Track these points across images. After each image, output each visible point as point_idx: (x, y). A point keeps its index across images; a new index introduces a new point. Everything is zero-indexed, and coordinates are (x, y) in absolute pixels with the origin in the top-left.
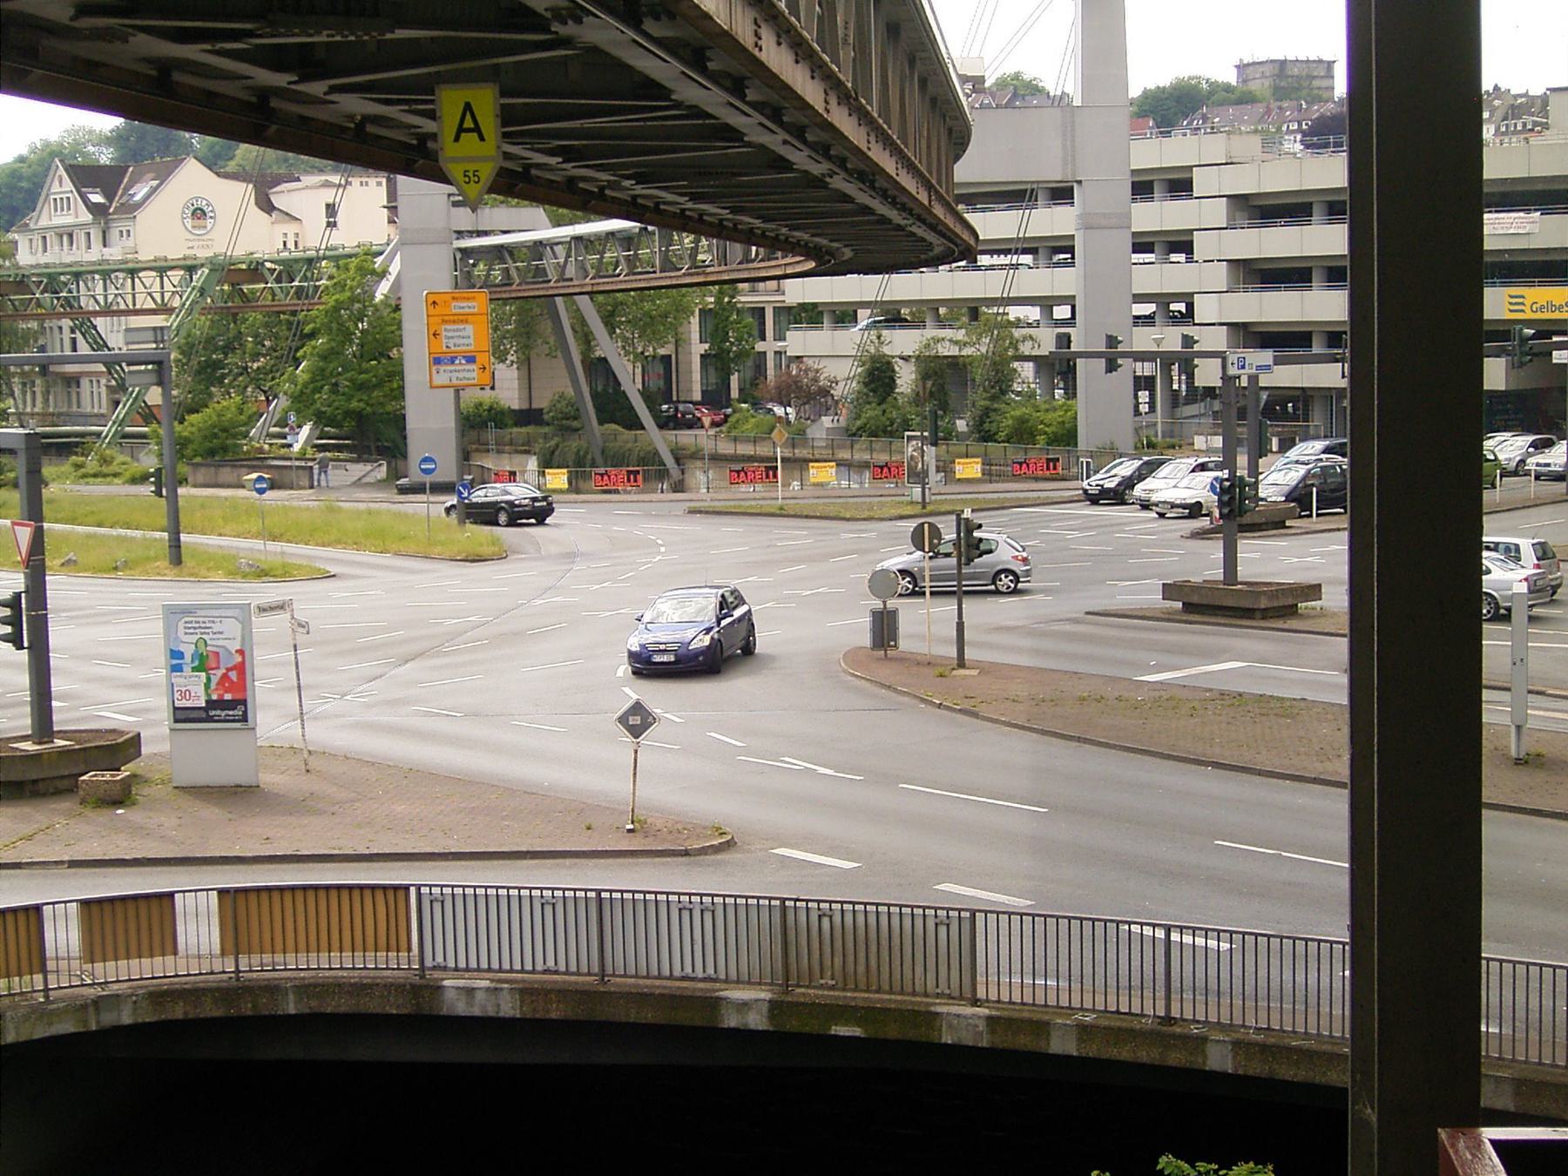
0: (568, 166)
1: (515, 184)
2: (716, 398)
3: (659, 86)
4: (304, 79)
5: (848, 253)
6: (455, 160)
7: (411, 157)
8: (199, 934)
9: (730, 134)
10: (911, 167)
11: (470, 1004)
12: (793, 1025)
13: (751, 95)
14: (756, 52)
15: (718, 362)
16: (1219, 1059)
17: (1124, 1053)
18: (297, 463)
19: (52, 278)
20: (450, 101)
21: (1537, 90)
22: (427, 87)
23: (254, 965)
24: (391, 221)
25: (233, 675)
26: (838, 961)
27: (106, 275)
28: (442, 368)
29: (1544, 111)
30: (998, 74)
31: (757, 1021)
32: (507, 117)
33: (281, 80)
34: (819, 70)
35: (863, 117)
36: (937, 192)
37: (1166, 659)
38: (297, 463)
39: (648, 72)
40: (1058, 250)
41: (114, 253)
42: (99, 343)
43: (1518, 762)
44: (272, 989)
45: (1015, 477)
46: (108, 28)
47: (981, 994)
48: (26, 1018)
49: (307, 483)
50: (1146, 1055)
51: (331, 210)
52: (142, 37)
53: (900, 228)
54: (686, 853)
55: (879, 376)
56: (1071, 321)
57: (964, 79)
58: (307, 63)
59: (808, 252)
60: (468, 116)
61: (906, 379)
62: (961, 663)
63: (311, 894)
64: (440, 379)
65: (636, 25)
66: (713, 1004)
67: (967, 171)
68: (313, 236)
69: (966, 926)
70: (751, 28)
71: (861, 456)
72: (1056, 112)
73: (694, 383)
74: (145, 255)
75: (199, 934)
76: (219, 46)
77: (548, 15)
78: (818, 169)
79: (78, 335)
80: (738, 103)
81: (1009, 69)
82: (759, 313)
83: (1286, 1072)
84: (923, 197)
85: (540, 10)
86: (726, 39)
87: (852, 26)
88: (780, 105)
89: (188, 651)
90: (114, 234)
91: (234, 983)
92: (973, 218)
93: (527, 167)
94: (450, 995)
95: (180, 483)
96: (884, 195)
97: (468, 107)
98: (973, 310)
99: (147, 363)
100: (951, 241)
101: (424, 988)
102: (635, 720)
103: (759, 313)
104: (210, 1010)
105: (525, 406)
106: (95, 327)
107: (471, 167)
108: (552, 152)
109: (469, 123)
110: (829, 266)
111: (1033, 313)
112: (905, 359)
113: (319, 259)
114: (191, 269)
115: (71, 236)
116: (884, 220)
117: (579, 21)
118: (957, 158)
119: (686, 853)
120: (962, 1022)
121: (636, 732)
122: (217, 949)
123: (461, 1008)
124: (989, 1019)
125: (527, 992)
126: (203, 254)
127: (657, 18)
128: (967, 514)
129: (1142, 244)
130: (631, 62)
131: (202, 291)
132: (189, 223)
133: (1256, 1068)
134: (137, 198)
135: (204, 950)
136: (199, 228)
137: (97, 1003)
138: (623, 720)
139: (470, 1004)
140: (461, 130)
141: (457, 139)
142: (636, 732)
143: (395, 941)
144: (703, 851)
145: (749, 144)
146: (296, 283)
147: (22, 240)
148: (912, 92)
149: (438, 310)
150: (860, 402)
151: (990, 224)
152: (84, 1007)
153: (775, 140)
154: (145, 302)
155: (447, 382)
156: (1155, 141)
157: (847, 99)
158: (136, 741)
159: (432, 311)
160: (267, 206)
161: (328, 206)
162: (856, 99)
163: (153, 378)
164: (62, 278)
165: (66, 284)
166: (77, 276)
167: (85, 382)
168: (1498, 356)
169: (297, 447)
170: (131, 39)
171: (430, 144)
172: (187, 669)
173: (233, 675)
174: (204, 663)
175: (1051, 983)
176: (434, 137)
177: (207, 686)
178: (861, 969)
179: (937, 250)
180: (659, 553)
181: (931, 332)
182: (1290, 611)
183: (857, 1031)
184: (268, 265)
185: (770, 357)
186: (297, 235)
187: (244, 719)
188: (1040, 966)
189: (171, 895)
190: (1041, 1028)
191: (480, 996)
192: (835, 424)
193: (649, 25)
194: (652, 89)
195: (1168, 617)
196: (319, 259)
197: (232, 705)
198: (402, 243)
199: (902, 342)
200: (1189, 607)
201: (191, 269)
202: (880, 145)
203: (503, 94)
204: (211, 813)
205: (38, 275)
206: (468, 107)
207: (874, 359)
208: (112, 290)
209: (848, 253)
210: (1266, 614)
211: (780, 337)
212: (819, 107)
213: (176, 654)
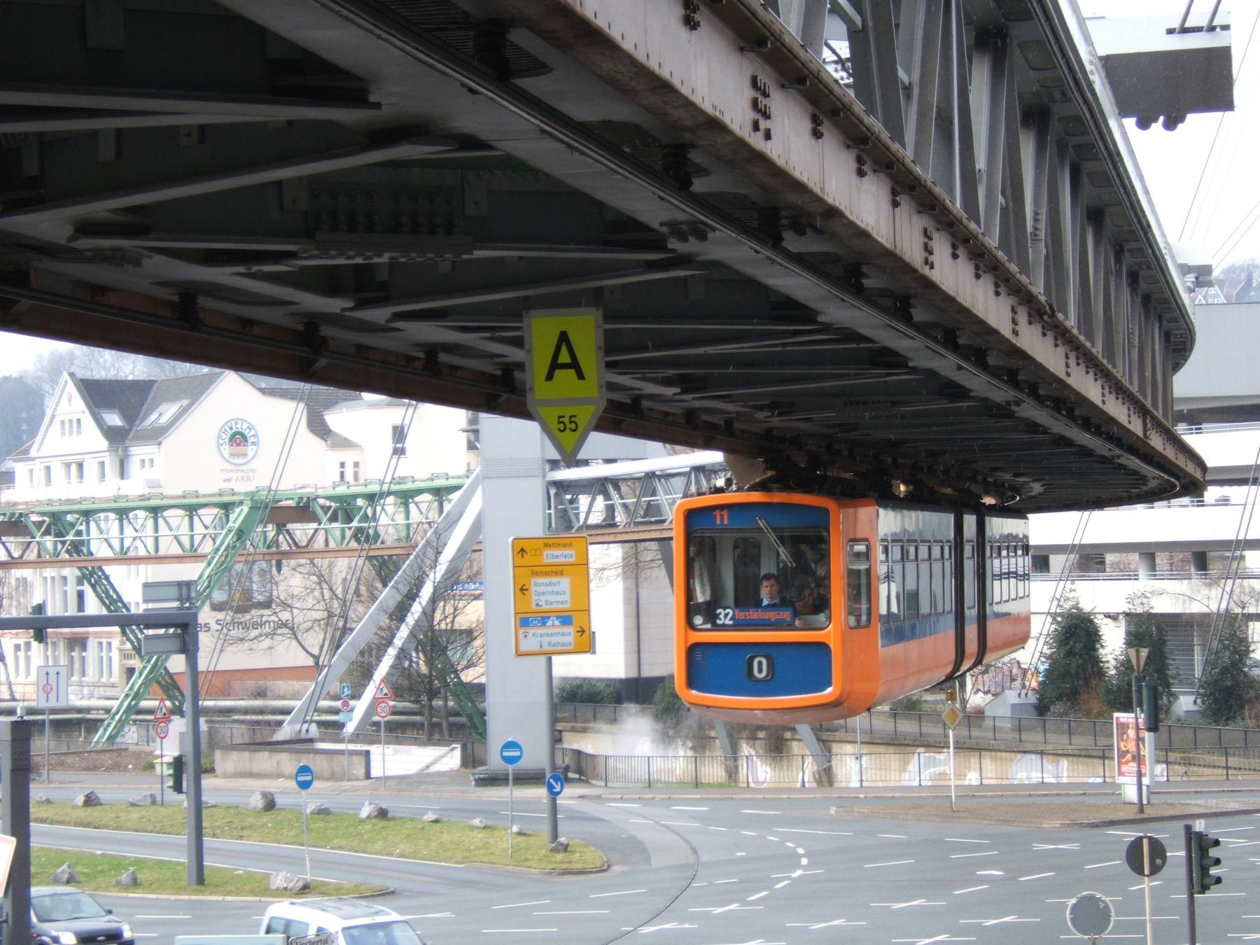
0: (689, 397)
1: (624, 417)
3: (803, 307)
4: (362, 304)
7: (495, 391)
9: (889, 359)
10: (1119, 390)
13: (918, 315)
14: (926, 271)
18: (352, 747)
19: (56, 517)
20: (542, 331)
22: (518, 310)
24: (472, 446)
27: (122, 514)
28: (531, 631)
30: (1224, 265)
32: (611, 346)
33: (333, 305)
34: (1005, 283)
35: (1062, 335)
36: (1154, 418)
38: (352, 747)
39: (787, 291)
41: (134, 487)
42: (112, 599)
46: (116, 250)
49: (362, 771)
51: (399, 433)
52: (159, 259)
53: (1104, 460)
55: (1077, 633)
57: (1185, 269)
58: (364, 286)
60: (564, 349)
61: (1113, 643)
64: (529, 644)
65: (775, 241)
67: (1189, 383)
68: (375, 466)
70: (919, 240)
74: (174, 488)
76: (255, 269)
77: (665, 230)
78: (1000, 394)
79: (87, 588)
80: (901, 327)
84: (1136, 426)
85: (655, 224)
86: (890, 260)
87: (1043, 217)
88: (954, 327)
90: (134, 465)
92: (1194, 440)
93: (637, 400)
95: (278, 526)
96: (1086, 424)
97: (564, 338)
98: (1201, 558)
99: (167, 626)
100: (1171, 473)
105: (634, 675)
106: (107, 578)
107: (567, 411)
108: (667, 382)
109: (564, 358)
112: (1113, 617)
113: (383, 495)
114: (227, 507)
115: (80, 465)
116: (1085, 452)
117: (702, 237)
118: (1177, 367)
126: (243, 487)
127: (801, 231)
128: (1199, 826)
130: (770, 282)
131: (241, 534)
132: (226, 450)
134: (163, 420)
136: (239, 455)
140: (555, 366)
141: (550, 377)
145: (915, 370)
146: (355, 524)
147: (20, 469)
148: (1118, 286)
149: (528, 560)
151: (1216, 446)
153: (947, 365)
154: (169, 547)
155: (536, 648)
157: (1043, 315)
159: (521, 562)
160: (319, 429)
161: (395, 428)
162: (1053, 315)
163: (176, 644)
164: (69, 518)
165: (72, 525)
166: (87, 514)
167: (92, 643)
169: (350, 728)
170: (145, 261)
171: (517, 375)
176: (521, 366)
179: (1153, 484)
180: (799, 866)
181: (1144, 583)
184: (321, 501)
186: (356, 465)
192: (1023, 700)
193: (792, 242)
194: (793, 311)
196: (383, 495)
198: (485, 477)
199: (1104, 598)
201: (227, 507)
202: (1082, 368)
203: (608, 318)
205: (42, 514)
206: (564, 338)
208: (129, 531)
209: (1037, 488)
212: (1005, 330)
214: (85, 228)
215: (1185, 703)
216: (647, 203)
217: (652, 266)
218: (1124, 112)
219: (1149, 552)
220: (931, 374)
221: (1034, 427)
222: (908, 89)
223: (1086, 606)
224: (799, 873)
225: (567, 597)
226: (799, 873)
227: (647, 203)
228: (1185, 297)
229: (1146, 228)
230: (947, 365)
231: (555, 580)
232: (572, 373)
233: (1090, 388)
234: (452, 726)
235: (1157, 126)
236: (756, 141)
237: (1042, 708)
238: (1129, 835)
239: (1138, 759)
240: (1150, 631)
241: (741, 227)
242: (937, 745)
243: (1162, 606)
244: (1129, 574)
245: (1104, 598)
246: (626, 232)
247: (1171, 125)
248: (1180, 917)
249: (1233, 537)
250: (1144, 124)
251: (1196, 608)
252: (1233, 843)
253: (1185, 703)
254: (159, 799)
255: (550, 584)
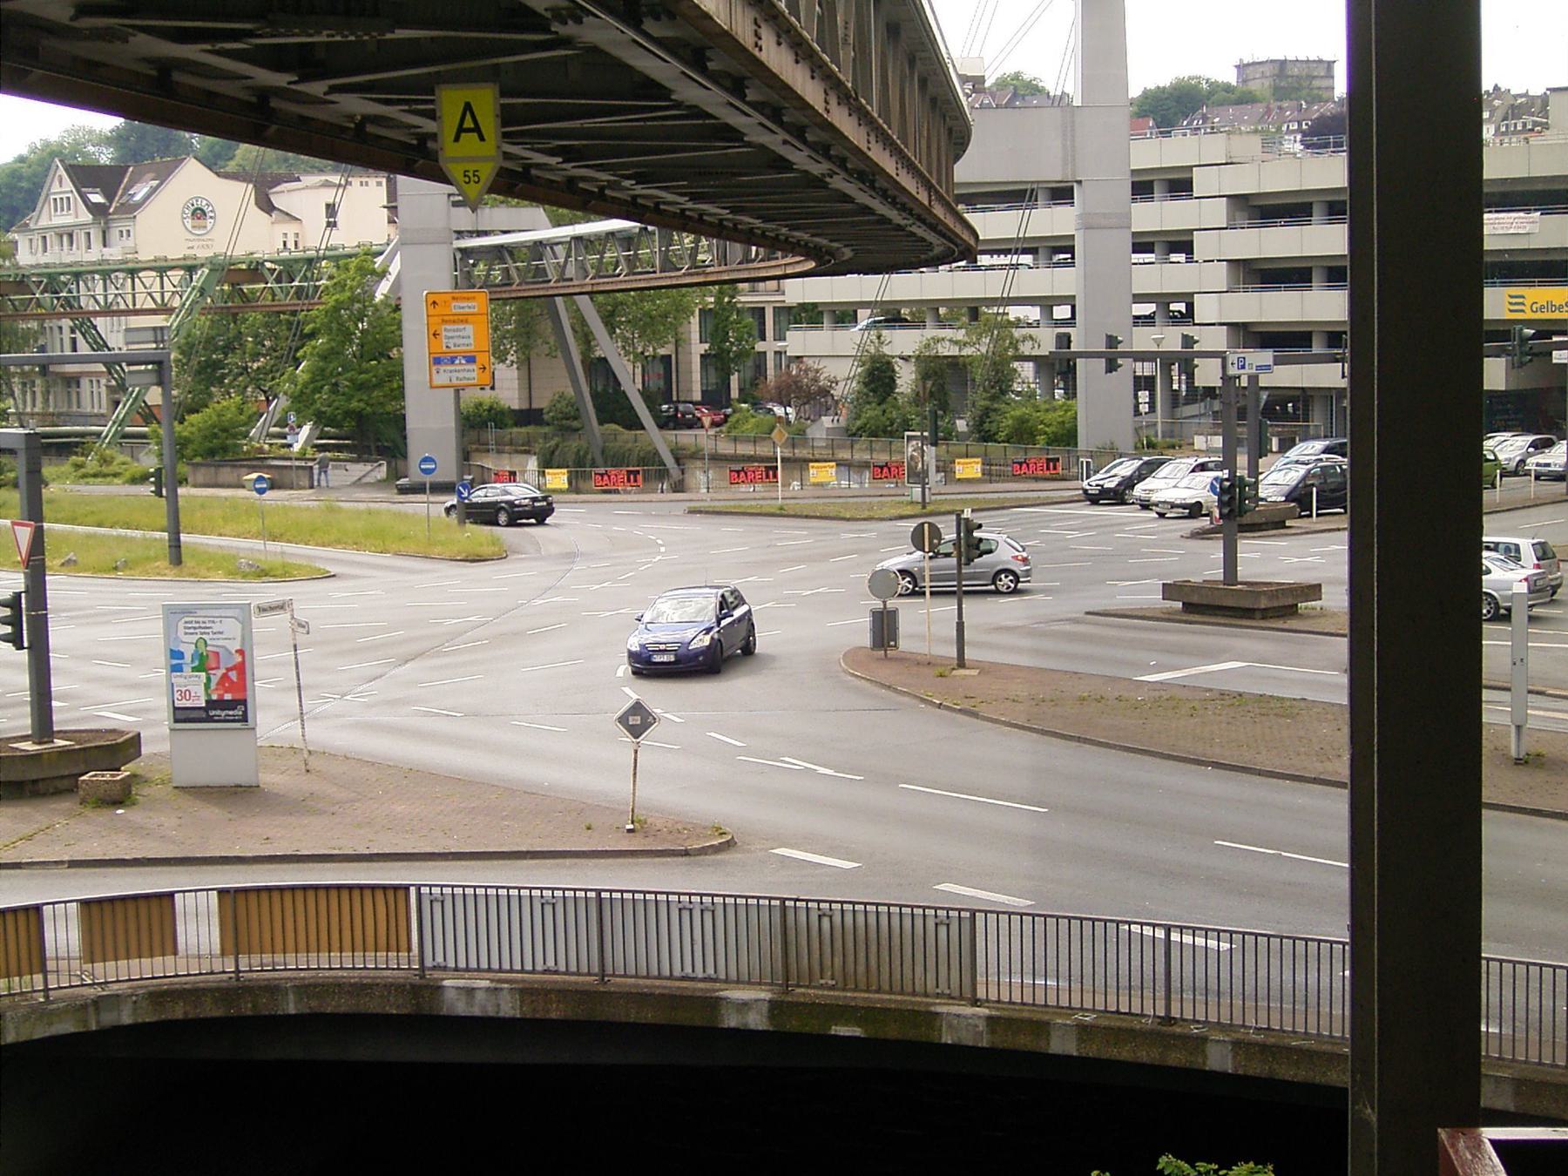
0: (568, 166)
1: (515, 184)
2: (716, 398)
3: (659, 86)
4: (304, 79)
5: (848, 253)
6: (455, 160)
7: (411, 157)
8: (199, 934)
9: (730, 134)
10: (911, 167)
11: (470, 1004)
12: (793, 1025)
13: (751, 95)
14: (756, 52)
15: (718, 362)
16: (1219, 1059)
17: (1124, 1053)
18: (297, 463)
19: (52, 278)
20: (450, 101)
21: (1537, 90)
22: (427, 87)
23: (254, 965)
24: (391, 221)
25: (233, 675)
26: (838, 961)
27: (106, 275)
28: (442, 368)
29: (1544, 111)
30: (998, 74)
31: (757, 1021)
32: (507, 117)
33: (281, 80)
34: (819, 70)
35: (863, 117)
36: (937, 192)
37: (1166, 659)
38: (297, 463)
39: (648, 72)
40: (1058, 250)
41: (114, 253)
42: (99, 343)
43: (1518, 762)
44: (272, 989)
45: (1015, 477)
46: (108, 28)
47: (981, 994)
48: (26, 1018)
49: (307, 483)
50: (1146, 1055)
51: (331, 210)
52: (142, 37)
53: (900, 228)
54: (686, 853)
55: (879, 376)
56: (1071, 321)
57: (964, 79)
58: (307, 63)
59: (808, 252)
60: (468, 116)
61: (906, 379)
62: (961, 663)
63: (311, 894)
64: (440, 379)
65: (636, 25)
66: (713, 1004)
67: (967, 171)
68: (313, 236)
69: (966, 926)
70: (751, 28)
71: (861, 456)
72: (1056, 112)
73: (694, 383)
74: (145, 255)
75: (199, 934)
76: (219, 46)
77: (548, 15)
78: (818, 169)
79: (78, 335)
80: (738, 103)
81: (1009, 69)
82: (759, 313)
83: (1286, 1072)
84: (923, 197)
85: (540, 10)
86: (726, 39)
87: (852, 26)
88: (780, 105)
89: (188, 651)
90: (114, 234)
91: (234, 983)
92: (973, 218)
93: (527, 167)
94: (450, 995)
95: (180, 483)
96: (884, 195)
97: (468, 107)
98: (973, 310)
99: (147, 363)
100: (951, 241)
101: (424, 988)
102: (635, 720)
103: (759, 313)
104: (210, 1010)
105: (525, 406)
106: (95, 327)
107: (471, 167)
108: (552, 152)
109: (469, 123)
110: (829, 266)
111: (1033, 313)
112: (905, 359)
113: (319, 259)
114: (191, 269)
115: (71, 236)
116: (884, 220)
117: (579, 21)
118: (957, 158)
119: (686, 853)
120: (962, 1022)
121: (636, 732)
122: (217, 949)
123: (461, 1008)
124: (989, 1019)
125: (527, 992)
126: (203, 254)
127: (657, 18)
128: (967, 514)
129: (1142, 244)
130: (631, 62)
131: (202, 291)
132: (189, 223)
133: (1256, 1068)
134: (137, 198)
135: (204, 950)
136: (199, 228)
137: (97, 1003)
138: (623, 720)
139: (470, 1004)
140: (461, 130)
141: (457, 139)
142: (636, 732)
143: (395, 941)
144: (703, 851)
145: (749, 144)
146: (296, 283)
147: (22, 240)
148: (912, 92)
149: (438, 310)
150: (860, 402)
151: (990, 224)
152: (84, 1007)
153: (775, 140)
154: (145, 302)
155: (447, 382)
156: (1155, 141)
157: (847, 99)
158: (136, 741)
159: (432, 311)
160: (267, 206)
161: (328, 206)
162: (856, 99)
163: (153, 378)
164: (62, 278)
165: (66, 284)
166: (77, 276)
167: (85, 382)
168: (1498, 356)
169: (297, 447)
170: (131, 39)
171: (430, 144)
172: (187, 669)
173: (233, 675)
174: (204, 663)
175: (1051, 983)
176: (434, 137)
177: (207, 686)
178: (861, 969)
179: (937, 250)
180: (659, 553)
181: (931, 332)
182: (1290, 611)
183: (857, 1031)
184: (268, 265)
185: (770, 357)
186: (297, 235)
187: (244, 719)
188: (1040, 966)
189: (171, 895)
190: (1041, 1028)
191: (480, 996)
192: (835, 424)
193: (649, 25)
194: (652, 89)
195: (1168, 617)
196: (319, 259)
197: (232, 705)
198: (402, 243)
199: (902, 342)
200: (1189, 607)
201: (191, 269)
202: (880, 145)
203: (503, 94)
204: (211, 813)
205: (38, 275)
206: (468, 107)
207: (874, 359)
208: (112, 290)
209: (848, 253)
210: (1266, 614)
211: (780, 337)
212: (819, 107)
213: (176, 654)
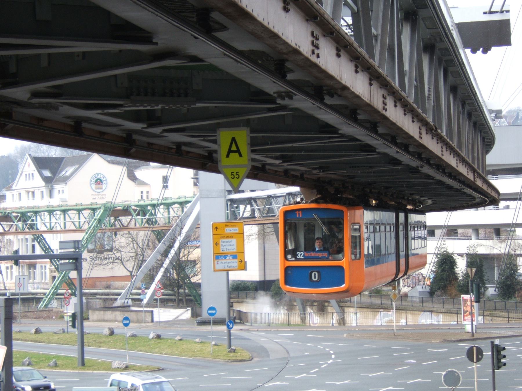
0: (285, 164)
1: (259, 173)
3: (333, 127)
4: (150, 126)
7: (205, 162)
9: (368, 149)
10: (464, 161)
13: (380, 130)
14: (384, 112)
18: (146, 309)
19: (23, 214)
20: (225, 137)
22: (214, 128)
24: (195, 185)
27: (51, 213)
28: (220, 261)
30: (507, 110)
32: (253, 143)
33: (138, 126)
34: (417, 117)
35: (440, 139)
36: (478, 173)
38: (146, 309)
39: (326, 121)
41: (56, 201)
42: (46, 248)
46: (48, 103)
49: (150, 319)
51: (165, 179)
52: (66, 107)
53: (457, 190)
55: (446, 262)
57: (491, 111)
58: (151, 119)
60: (234, 144)
61: (461, 266)
64: (219, 266)
65: (321, 100)
67: (493, 158)
68: (155, 193)
70: (381, 99)
74: (72, 202)
76: (106, 111)
77: (275, 95)
78: (414, 163)
79: (36, 243)
80: (373, 135)
84: (471, 176)
85: (271, 93)
86: (369, 107)
87: (432, 90)
88: (395, 136)
90: (55, 193)
92: (495, 182)
93: (264, 165)
95: (115, 217)
96: (450, 176)
97: (234, 140)
98: (498, 231)
99: (69, 259)
100: (485, 196)
105: (262, 279)
106: (44, 239)
107: (235, 170)
108: (276, 158)
109: (234, 148)
112: (461, 255)
113: (158, 205)
114: (94, 210)
115: (33, 193)
116: (449, 187)
117: (291, 98)
118: (487, 152)
126: (101, 202)
127: (332, 96)
128: (497, 342)
130: (319, 116)
131: (100, 221)
132: (94, 186)
134: (68, 174)
136: (99, 188)
140: (230, 151)
141: (228, 156)
145: (379, 153)
146: (147, 217)
147: (8, 194)
148: (463, 118)
149: (219, 232)
151: (504, 184)
153: (392, 151)
154: (70, 226)
155: (222, 268)
157: (432, 130)
159: (216, 232)
160: (132, 177)
161: (164, 177)
162: (436, 130)
163: (73, 266)
164: (29, 214)
165: (30, 217)
166: (36, 213)
167: (38, 266)
169: (145, 301)
170: (60, 108)
171: (214, 155)
176: (216, 151)
179: (477, 200)
180: (331, 358)
181: (474, 241)
184: (133, 207)
186: (148, 192)
192: (424, 290)
193: (328, 100)
194: (328, 129)
196: (158, 205)
198: (201, 198)
199: (457, 247)
201: (94, 210)
202: (448, 152)
203: (252, 131)
205: (18, 213)
206: (234, 140)
208: (53, 220)
209: (430, 202)
212: (416, 136)
214: (35, 94)
215: (491, 291)
216: (268, 84)
217: (270, 110)
218: (466, 46)
219: (476, 229)
220: (386, 155)
221: (428, 177)
222: (376, 37)
223: (450, 251)
224: (331, 361)
225: (235, 247)
226: (331, 361)
227: (268, 84)
228: (491, 123)
229: (475, 95)
230: (392, 151)
231: (230, 240)
232: (237, 154)
233: (452, 161)
234: (187, 300)
235: (480, 52)
236: (313, 58)
237: (432, 293)
238: (468, 345)
239: (472, 314)
240: (476, 261)
241: (307, 94)
242: (388, 308)
243: (482, 251)
244: (468, 238)
245: (457, 247)
246: (259, 96)
247: (485, 52)
248: (489, 379)
249: (511, 222)
250: (474, 51)
251: (495, 252)
252: (511, 349)
253: (491, 291)
254: (66, 330)
255: (228, 242)
